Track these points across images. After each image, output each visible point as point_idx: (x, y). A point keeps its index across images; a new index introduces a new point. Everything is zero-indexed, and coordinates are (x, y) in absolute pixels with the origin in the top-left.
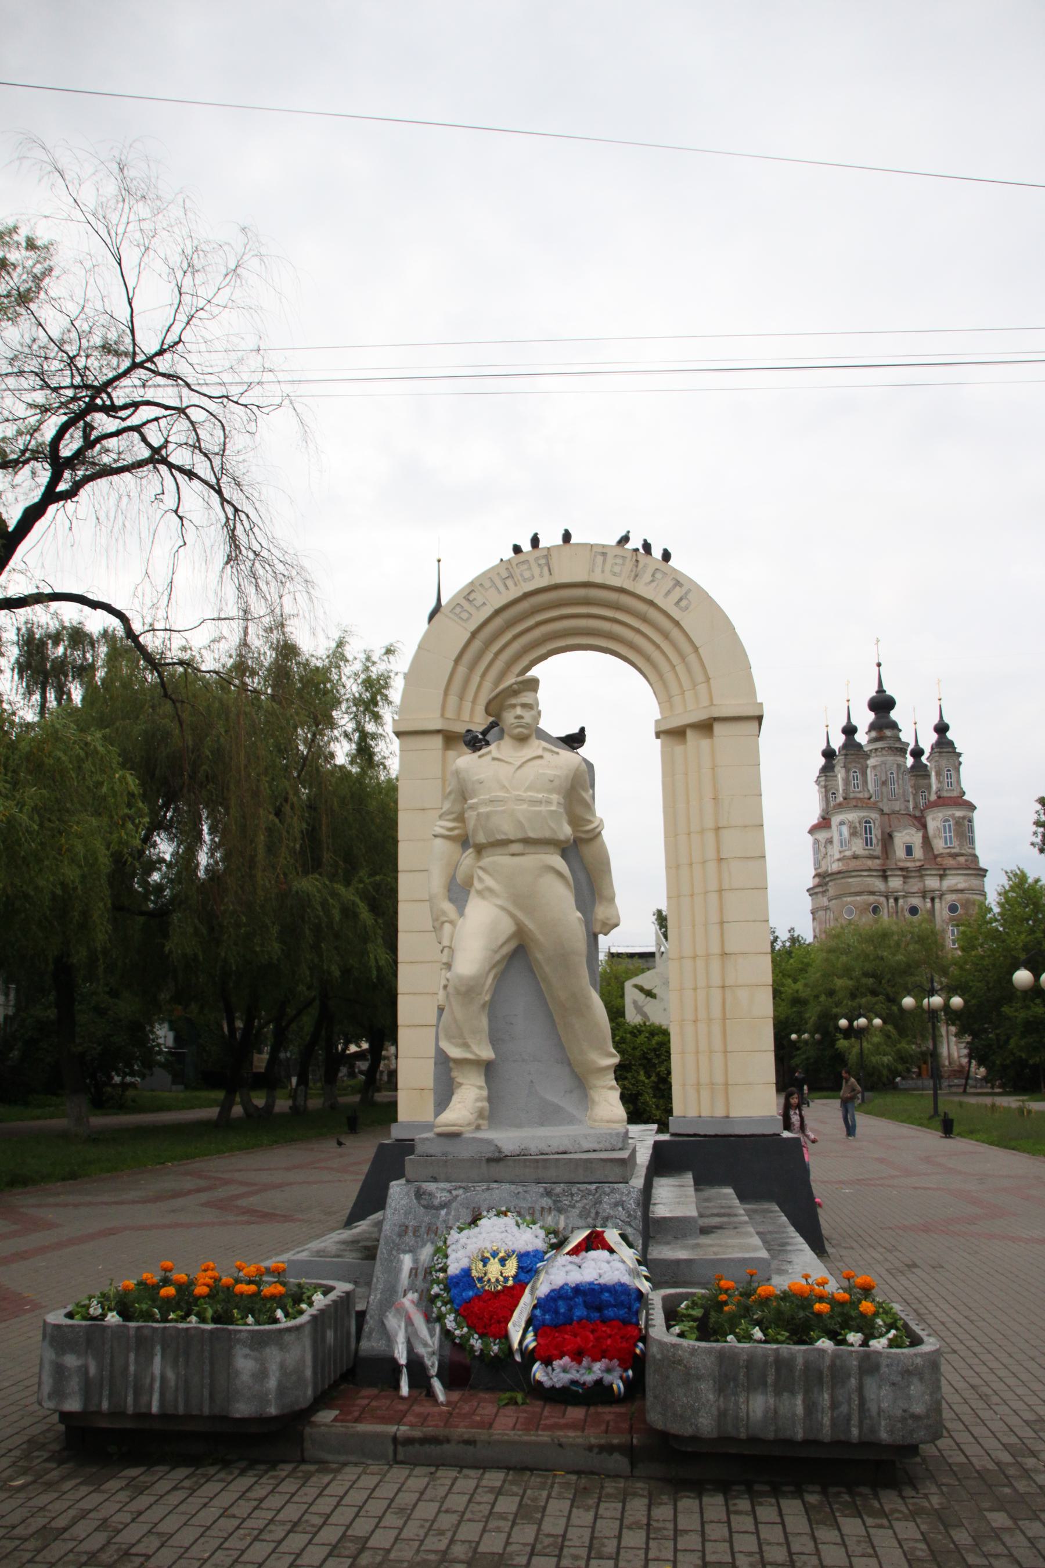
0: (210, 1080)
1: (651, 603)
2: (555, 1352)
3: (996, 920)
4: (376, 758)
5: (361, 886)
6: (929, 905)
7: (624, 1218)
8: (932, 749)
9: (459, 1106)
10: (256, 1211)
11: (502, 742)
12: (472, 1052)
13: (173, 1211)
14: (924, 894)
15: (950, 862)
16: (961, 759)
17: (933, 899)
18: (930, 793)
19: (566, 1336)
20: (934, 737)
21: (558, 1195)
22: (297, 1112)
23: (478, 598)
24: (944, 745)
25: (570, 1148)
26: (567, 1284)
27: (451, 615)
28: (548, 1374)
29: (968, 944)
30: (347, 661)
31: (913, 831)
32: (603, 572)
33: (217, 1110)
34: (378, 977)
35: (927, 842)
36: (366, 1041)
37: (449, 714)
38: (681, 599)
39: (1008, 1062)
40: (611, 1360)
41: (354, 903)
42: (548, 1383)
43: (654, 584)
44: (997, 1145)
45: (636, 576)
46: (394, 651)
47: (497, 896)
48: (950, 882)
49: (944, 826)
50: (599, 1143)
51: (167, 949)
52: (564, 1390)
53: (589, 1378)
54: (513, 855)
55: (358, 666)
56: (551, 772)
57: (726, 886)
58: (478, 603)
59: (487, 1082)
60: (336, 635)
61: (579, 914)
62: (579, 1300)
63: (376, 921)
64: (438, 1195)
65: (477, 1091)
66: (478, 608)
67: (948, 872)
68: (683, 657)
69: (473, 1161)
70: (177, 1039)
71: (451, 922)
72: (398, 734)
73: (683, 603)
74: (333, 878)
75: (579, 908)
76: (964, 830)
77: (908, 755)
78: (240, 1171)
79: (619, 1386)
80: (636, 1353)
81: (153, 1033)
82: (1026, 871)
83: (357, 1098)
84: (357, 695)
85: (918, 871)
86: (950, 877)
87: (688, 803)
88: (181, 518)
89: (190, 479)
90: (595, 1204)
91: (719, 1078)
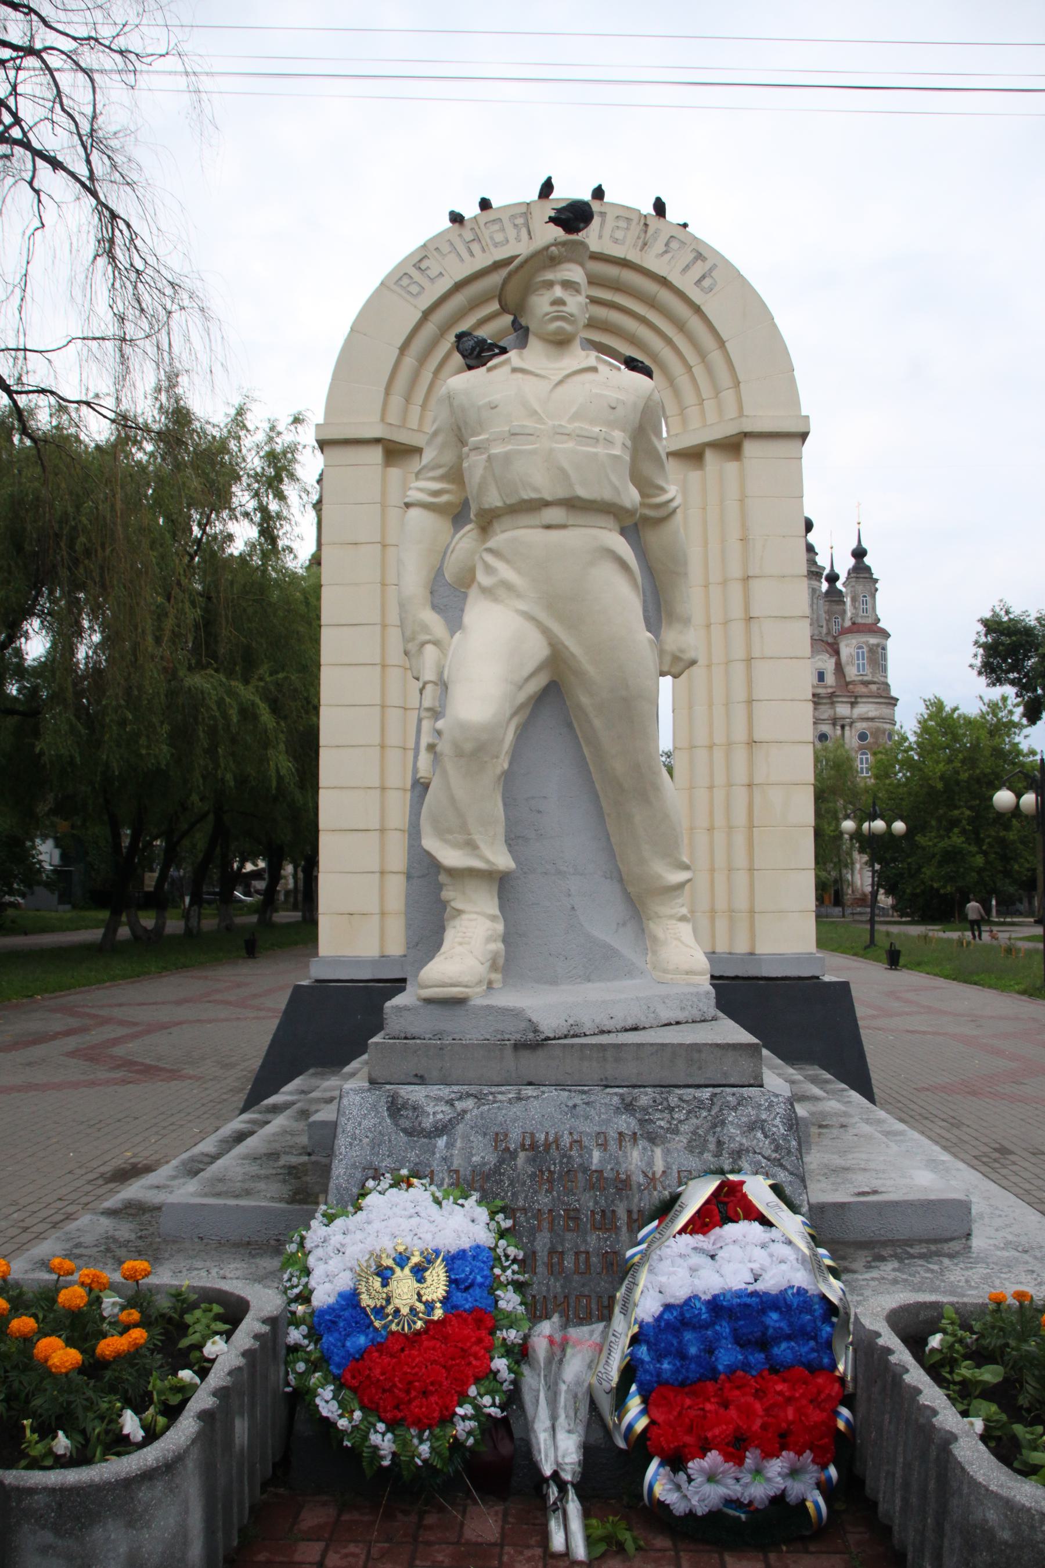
0: (98, 899)
1: (664, 282)
2: (688, 1439)
3: (912, 749)
4: (281, 544)
5: (262, 684)
6: (839, 732)
7: (768, 1152)
8: (849, 573)
9: (459, 949)
10: (135, 1063)
11: (525, 351)
12: (482, 858)
13: (30, 1064)
14: (834, 721)
15: (862, 690)
16: (877, 586)
17: (843, 727)
18: (843, 620)
19: (708, 1407)
20: (851, 562)
21: (645, 1110)
22: (191, 935)
23: (433, 266)
24: (861, 571)
25: (643, 1021)
26: (696, 1297)
27: (394, 287)
28: (678, 1488)
29: (883, 772)
30: (248, 430)
31: (826, 656)
32: (600, 237)
33: (102, 931)
34: (278, 788)
35: (839, 668)
36: (263, 860)
37: (393, 418)
38: (703, 277)
39: (918, 891)
40: (799, 1453)
41: (253, 704)
42: (679, 1508)
43: (668, 257)
44: (954, 979)
45: (645, 244)
46: (303, 420)
47: (519, 596)
48: (861, 710)
49: (858, 653)
50: (682, 1009)
51: (37, 750)
52: (714, 1517)
53: (758, 1491)
54: (548, 527)
55: (260, 437)
56: (613, 395)
57: (756, 654)
58: (433, 273)
59: (502, 908)
60: (237, 401)
61: (649, 634)
62: (724, 1328)
63: (278, 723)
64: (430, 1110)
65: (488, 924)
66: (432, 280)
67: (859, 700)
68: (702, 355)
69: (492, 1048)
70: (63, 857)
71: (436, 643)
72: (323, 444)
73: (706, 283)
74: (230, 674)
75: (649, 631)
76: (877, 658)
77: (823, 580)
78: (121, 1005)
79: (816, 1502)
80: (839, 1430)
81: (34, 847)
82: (943, 699)
83: (254, 919)
84: (259, 470)
85: (830, 697)
86: (861, 705)
87: (706, 544)
88: (37, 192)
89: (54, 169)
90: (714, 1126)
91: (741, 902)
